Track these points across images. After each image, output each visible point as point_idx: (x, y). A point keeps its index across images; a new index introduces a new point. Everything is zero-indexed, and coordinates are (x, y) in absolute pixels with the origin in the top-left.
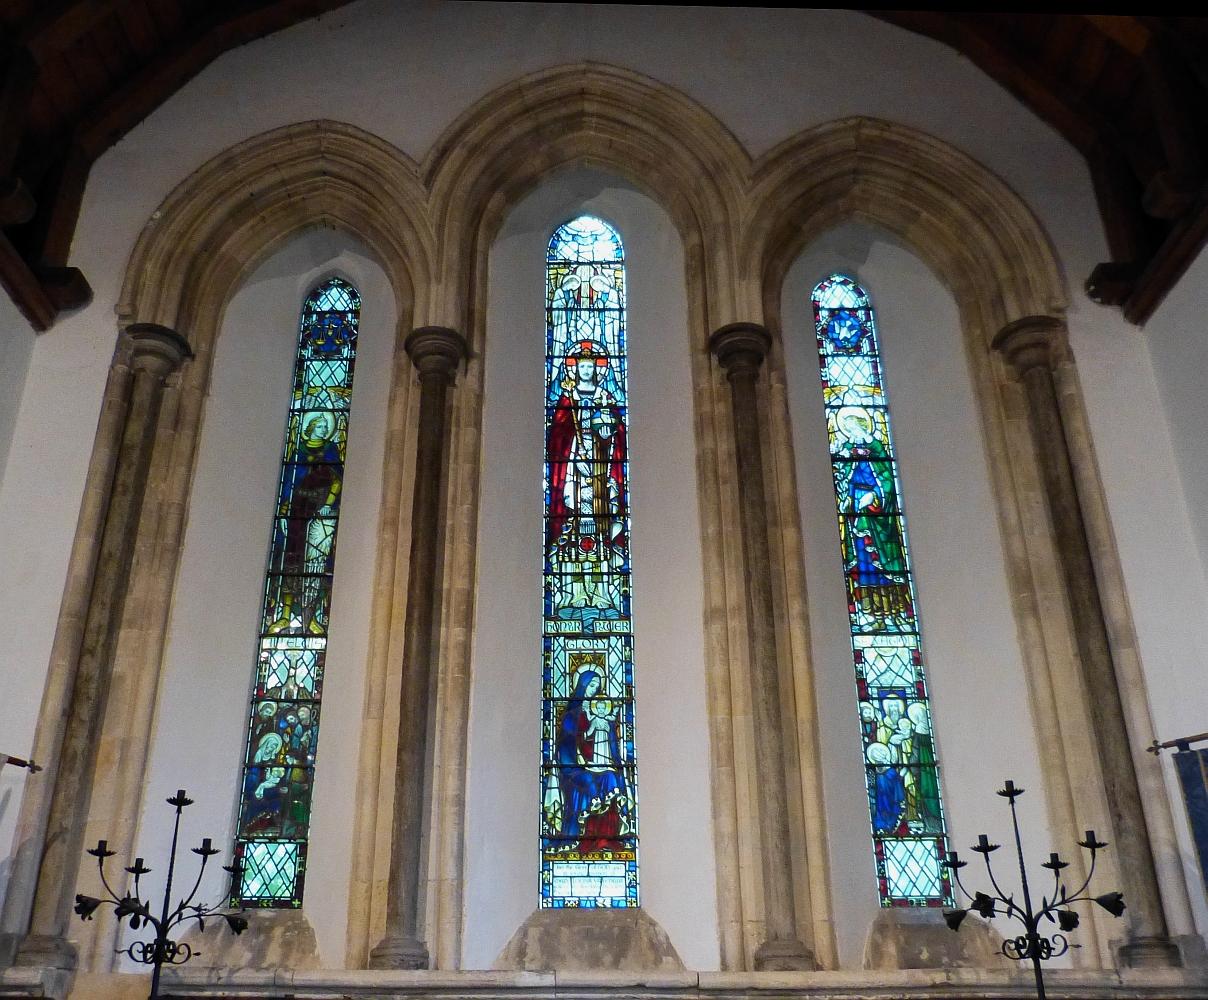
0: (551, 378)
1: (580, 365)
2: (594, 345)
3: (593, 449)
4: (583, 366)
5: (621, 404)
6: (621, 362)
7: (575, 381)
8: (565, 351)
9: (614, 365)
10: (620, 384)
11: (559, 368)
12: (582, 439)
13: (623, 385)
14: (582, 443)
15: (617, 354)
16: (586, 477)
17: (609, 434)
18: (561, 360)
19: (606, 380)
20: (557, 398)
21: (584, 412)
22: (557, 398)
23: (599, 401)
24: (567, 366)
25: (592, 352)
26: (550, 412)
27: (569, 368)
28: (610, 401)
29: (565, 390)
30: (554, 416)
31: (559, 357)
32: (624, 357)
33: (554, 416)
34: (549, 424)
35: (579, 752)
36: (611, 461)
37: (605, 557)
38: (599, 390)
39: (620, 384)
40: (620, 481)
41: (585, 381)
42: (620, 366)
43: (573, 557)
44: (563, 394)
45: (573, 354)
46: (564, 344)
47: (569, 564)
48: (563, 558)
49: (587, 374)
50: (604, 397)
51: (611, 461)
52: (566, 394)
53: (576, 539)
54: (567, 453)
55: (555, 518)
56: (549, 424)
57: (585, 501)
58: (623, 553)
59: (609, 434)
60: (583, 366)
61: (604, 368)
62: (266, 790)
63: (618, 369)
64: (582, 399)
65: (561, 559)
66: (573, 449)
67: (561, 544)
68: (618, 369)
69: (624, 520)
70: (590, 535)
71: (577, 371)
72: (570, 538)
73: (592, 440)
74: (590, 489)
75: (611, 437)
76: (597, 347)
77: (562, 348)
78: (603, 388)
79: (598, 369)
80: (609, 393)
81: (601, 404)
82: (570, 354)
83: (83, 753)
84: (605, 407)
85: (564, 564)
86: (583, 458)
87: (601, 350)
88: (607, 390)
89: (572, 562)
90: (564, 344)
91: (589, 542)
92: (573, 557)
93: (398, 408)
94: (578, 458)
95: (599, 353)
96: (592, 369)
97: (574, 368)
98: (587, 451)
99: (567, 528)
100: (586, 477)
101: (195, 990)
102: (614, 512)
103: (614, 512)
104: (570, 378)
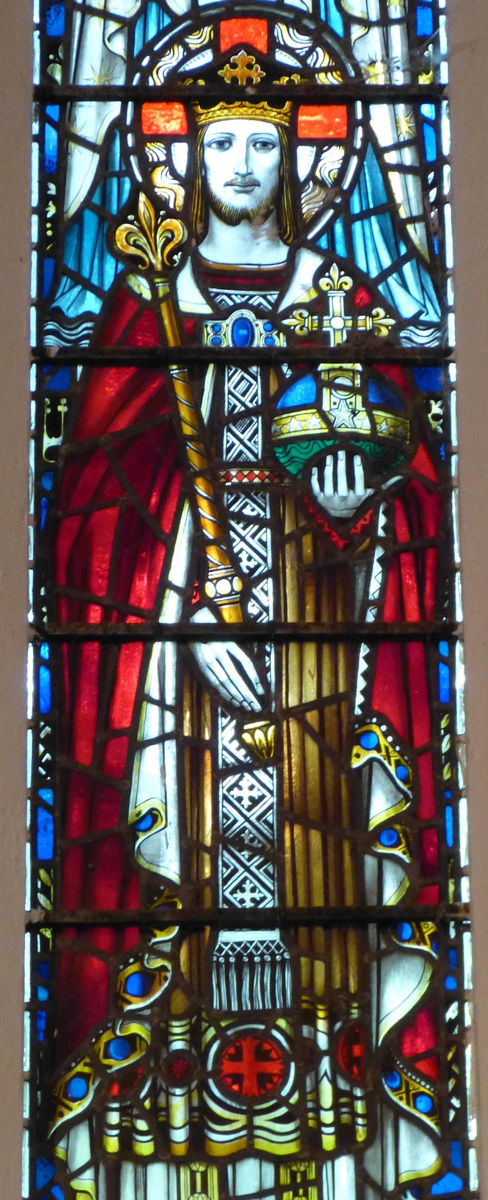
0: (60, 199)
1: (212, 133)
2: (282, 32)
3: (276, 573)
4: (224, 144)
5: (423, 338)
6: (420, 121)
7: (183, 215)
8: (132, 63)
9: (385, 138)
10: (416, 233)
11: (103, 150)
12: (223, 518)
13: (435, 233)
14: (224, 539)
15: (399, 78)
16: (242, 715)
17: (361, 491)
18: (114, 109)
19: (344, 213)
20: (92, 304)
21: (234, 379)
22: (92, 304)
23: (311, 323)
24: (142, 140)
25: (275, 70)
26: (55, 383)
27: (155, 151)
28: (365, 323)
29: (133, 264)
30: (79, 405)
31: (102, 94)
32: (434, 94)
33: (79, 405)
34: (49, 442)
35: (321, 1014)
36: (373, 636)
37: (345, 1134)
38: (309, 263)
39: (416, 233)
40: (420, 738)
41: (233, 219)
42: (417, 142)
43: (179, 1135)
44: (120, 278)
45: (174, 75)
46: (128, 25)
47: (157, 1173)
48: (127, 1136)
49: (248, 184)
50: (337, 303)
51: (373, 636)
52: (141, 286)
53: (195, 1035)
54: (142, 584)
55: (80, 928)
56: (49, 442)
57: (238, 842)
58: (438, 1109)
59: (361, 491)
60: (224, 144)
61: (334, 156)
62: (384, 528)
63: (408, 157)
64: (221, 313)
65: (112, 1145)
66: (178, 573)
67: (117, 1065)
68: (408, 157)
69: (439, 939)
70: (267, 1016)
71: (197, 165)
72: (162, 1036)
73: (276, 524)
74: (267, 778)
75: (367, 507)
76: (300, 42)
77: (119, 45)
78: (329, 257)
79: (305, 155)
80: (361, 279)
81: (319, 337)
82: (157, 79)
83: (136, 661)
84: (338, 355)
85: (128, 1172)
86: (229, 615)
87: (321, 59)
88: (348, 266)
89: (177, 1162)
90: (128, 25)
91: (262, 1055)
92: (179, 1135)
93: (346, 512)
94: (204, 617)
95: (308, 72)
96: (273, 156)
97: (180, 152)
98: (250, 581)
99: (148, 979)
100: (242, 715)
101: (191, 769)
102: (391, 896)
103: (391, 896)
104: (158, 203)
